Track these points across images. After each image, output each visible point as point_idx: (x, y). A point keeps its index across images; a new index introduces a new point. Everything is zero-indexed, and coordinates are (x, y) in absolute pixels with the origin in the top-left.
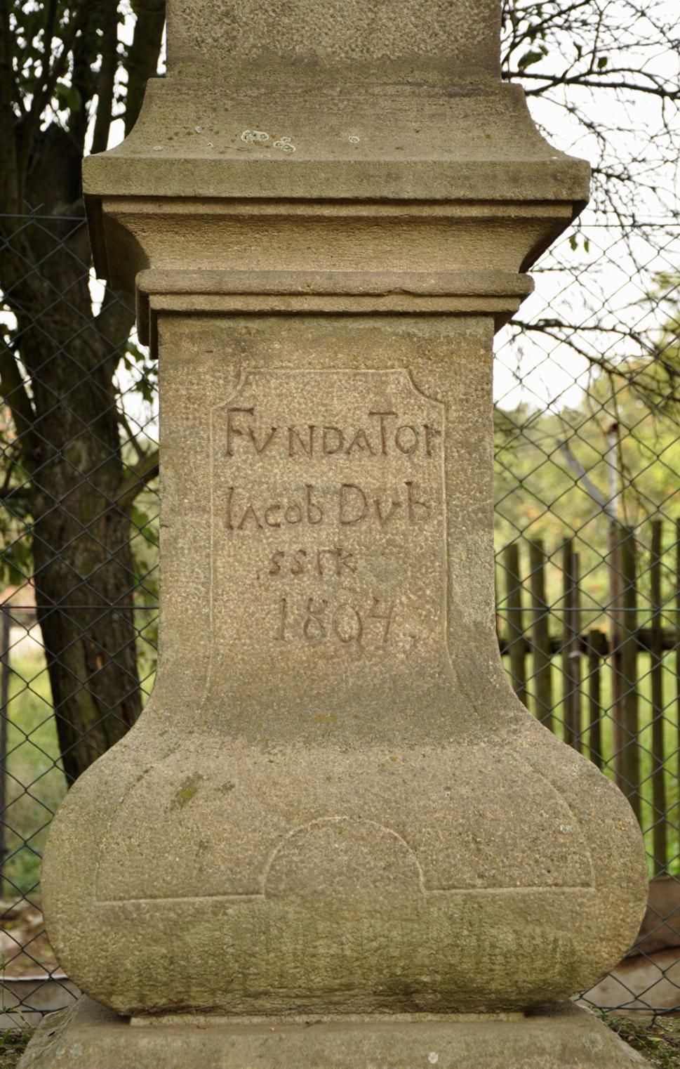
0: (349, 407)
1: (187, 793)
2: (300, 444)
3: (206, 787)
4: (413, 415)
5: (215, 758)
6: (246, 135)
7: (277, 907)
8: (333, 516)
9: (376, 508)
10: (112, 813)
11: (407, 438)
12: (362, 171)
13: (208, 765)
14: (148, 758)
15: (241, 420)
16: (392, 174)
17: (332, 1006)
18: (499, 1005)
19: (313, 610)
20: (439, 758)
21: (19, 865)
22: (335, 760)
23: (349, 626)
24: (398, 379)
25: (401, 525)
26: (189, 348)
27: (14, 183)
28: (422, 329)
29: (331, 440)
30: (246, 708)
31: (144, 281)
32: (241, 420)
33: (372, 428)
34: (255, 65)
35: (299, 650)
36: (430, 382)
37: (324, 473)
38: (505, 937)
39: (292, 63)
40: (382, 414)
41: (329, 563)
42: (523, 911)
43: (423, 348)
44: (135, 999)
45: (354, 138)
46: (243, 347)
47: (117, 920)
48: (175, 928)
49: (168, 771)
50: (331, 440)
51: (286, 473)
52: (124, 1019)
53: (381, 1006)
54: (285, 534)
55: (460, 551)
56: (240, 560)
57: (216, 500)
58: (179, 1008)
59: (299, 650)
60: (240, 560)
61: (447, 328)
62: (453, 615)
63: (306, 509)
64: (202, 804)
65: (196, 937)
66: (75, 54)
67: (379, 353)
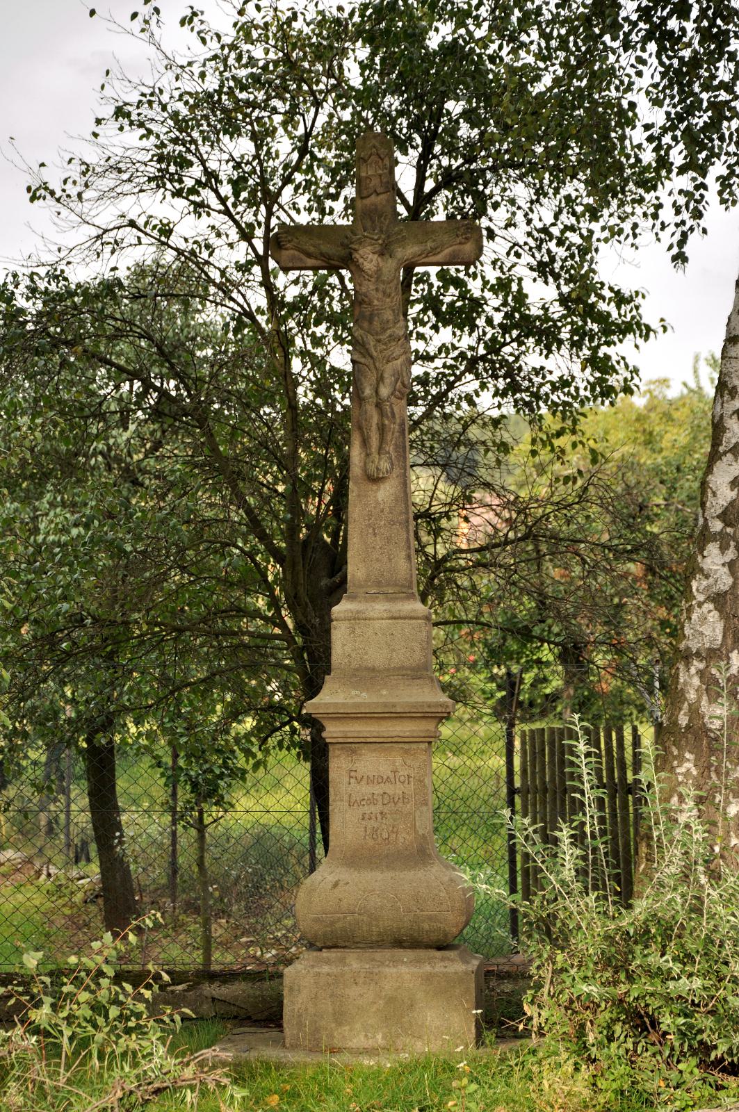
0: (385, 770)
1: (336, 885)
2: (370, 781)
3: (341, 883)
4: (403, 772)
5: (344, 874)
6: (354, 692)
7: (361, 917)
8: (380, 802)
9: (393, 800)
10: (314, 890)
11: (402, 779)
12: (385, 704)
13: (342, 877)
14: (325, 875)
15: (353, 774)
16: (394, 706)
17: (379, 947)
18: (428, 946)
19: (375, 830)
20: (409, 875)
21: (692, 692)
22: (378, 875)
23: (385, 835)
24: (399, 761)
25: (400, 805)
26: (337, 752)
27: (301, 575)
28: (406, 746)
29: (381, 780)
30: (358, 859)
31: (324, 735)
32: (353, 774)
33: (392, 775)
34: (357, 670)
35: (371, 842)
36: (409, 762)
37: (378, 790)
38: (426, 926)
39: (368, 669)
40: (395, 772)
41: (379, 816)
42: (430, 918)
43: (407, 752)
44: (614, 1021)
45: (384, 692)
46: (354, 752)
47: (316, 920)
48: (332, 923)
49: (331, 879)
50: (381, 780)
51: (366, 790)
52: (320, 950)
53: (394, 947)
54: (366, 807)
55: (418, 813)
56: (352, 816)
57: (346, 798)
58: (335, 947)
59: (371, 842)
60: (352, 816)
61: (414, 746)
62: (416, 832)
63: (372, 801)
64: (339, 888)
65: (339, 925)
66: (325, 542)
67: (394, 753)
